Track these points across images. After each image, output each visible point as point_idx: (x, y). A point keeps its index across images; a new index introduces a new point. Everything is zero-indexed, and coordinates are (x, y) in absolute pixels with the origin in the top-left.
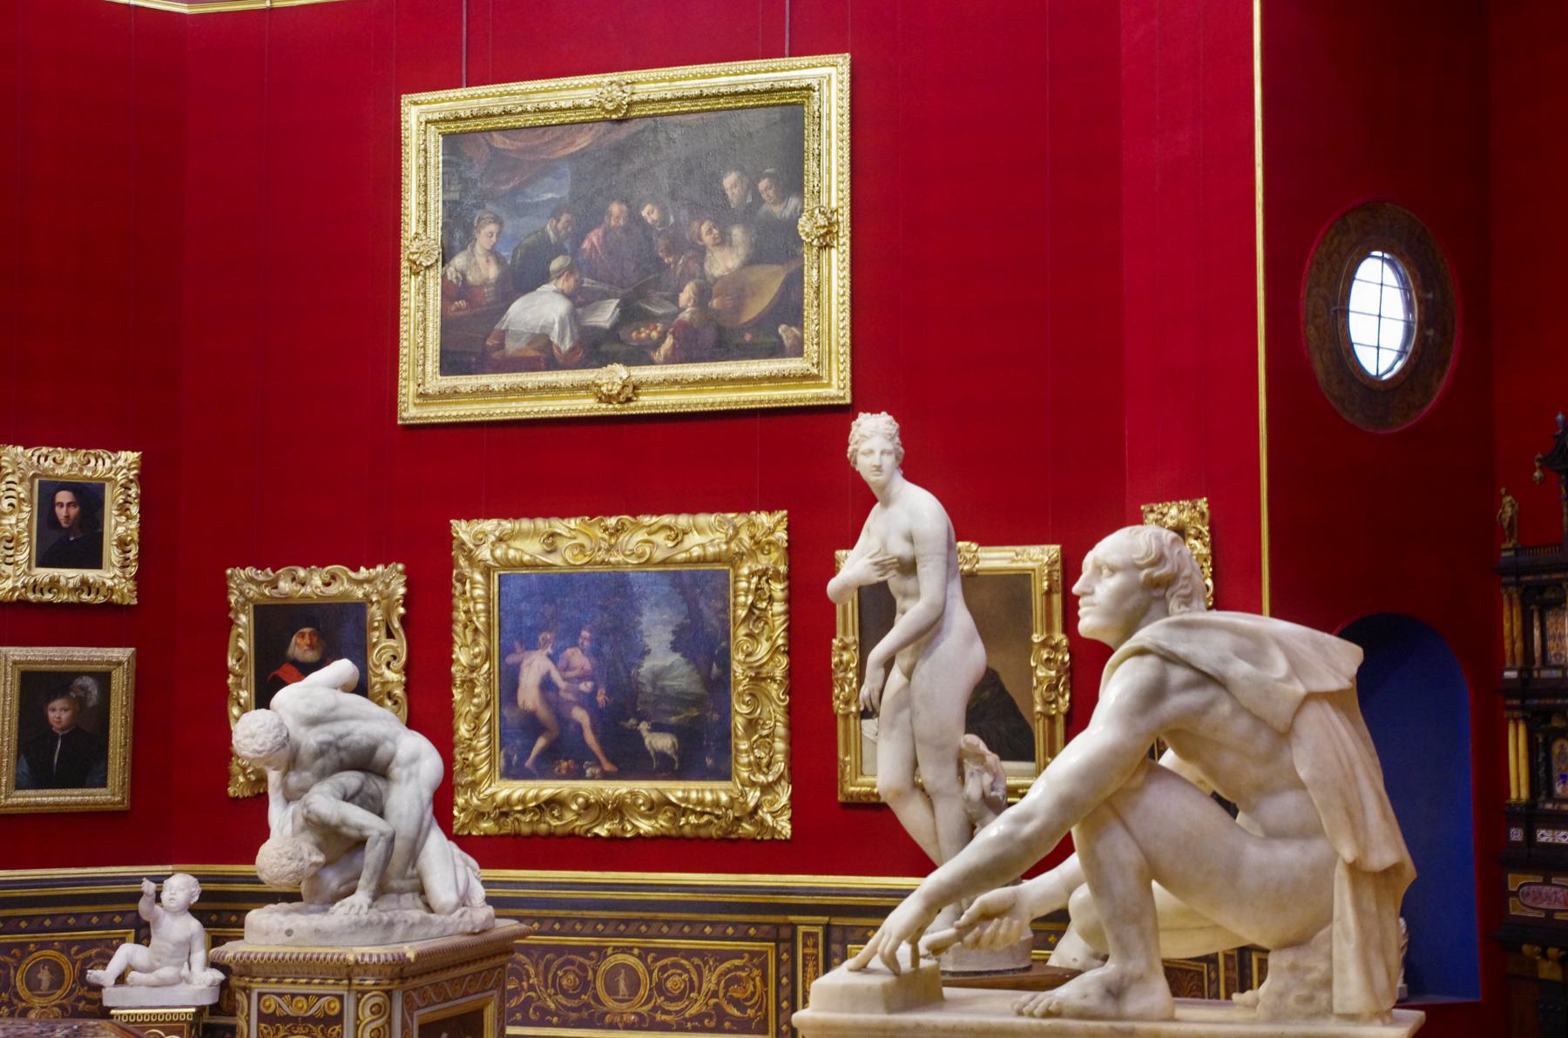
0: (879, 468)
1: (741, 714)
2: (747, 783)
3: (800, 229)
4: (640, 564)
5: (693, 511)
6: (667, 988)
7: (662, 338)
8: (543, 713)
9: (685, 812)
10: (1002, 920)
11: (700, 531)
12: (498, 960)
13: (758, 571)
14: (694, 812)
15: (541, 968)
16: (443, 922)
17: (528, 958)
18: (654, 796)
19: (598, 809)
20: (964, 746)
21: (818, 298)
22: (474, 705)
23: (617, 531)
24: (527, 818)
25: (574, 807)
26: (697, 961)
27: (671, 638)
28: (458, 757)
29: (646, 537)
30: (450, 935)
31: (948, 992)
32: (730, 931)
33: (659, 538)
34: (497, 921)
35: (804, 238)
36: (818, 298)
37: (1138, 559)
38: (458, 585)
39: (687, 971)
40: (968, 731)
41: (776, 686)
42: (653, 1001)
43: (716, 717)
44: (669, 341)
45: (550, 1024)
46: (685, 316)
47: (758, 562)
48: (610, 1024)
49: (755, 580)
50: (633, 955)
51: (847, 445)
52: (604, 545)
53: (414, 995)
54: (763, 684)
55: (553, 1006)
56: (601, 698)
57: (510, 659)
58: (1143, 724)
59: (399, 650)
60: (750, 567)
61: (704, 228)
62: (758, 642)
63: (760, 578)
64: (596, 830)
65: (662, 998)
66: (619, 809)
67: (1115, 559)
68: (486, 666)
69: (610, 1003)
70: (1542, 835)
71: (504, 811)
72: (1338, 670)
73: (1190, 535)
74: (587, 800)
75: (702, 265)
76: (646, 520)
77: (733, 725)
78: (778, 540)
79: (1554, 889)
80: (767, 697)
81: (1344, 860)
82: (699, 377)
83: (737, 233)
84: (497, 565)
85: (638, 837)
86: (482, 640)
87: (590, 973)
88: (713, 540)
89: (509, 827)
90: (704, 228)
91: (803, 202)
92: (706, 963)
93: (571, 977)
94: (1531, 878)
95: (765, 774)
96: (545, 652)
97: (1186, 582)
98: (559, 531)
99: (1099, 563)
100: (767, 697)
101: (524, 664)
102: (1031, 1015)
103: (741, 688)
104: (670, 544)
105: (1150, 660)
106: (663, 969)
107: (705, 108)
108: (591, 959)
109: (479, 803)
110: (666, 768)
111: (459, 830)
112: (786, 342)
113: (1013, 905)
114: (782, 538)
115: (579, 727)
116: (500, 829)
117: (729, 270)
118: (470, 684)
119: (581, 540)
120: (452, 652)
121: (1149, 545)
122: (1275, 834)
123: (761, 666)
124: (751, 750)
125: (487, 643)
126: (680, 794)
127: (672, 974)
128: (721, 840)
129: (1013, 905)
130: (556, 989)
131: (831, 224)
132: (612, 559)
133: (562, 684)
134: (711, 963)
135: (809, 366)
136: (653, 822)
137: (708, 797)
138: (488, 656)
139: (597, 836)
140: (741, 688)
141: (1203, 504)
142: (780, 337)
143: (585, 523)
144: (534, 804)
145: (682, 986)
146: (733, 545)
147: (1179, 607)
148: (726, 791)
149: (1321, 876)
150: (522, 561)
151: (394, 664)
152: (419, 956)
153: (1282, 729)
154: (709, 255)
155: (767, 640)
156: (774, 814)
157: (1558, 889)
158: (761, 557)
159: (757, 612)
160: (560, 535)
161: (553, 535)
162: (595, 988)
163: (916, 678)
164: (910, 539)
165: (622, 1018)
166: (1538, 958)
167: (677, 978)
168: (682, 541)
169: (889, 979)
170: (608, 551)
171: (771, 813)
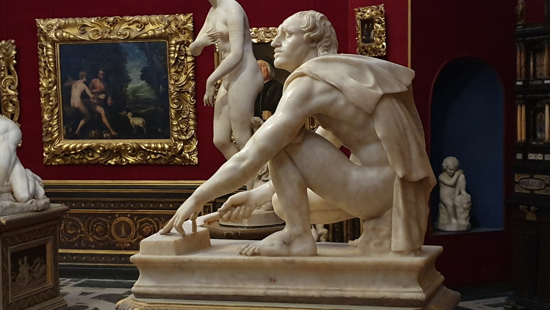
1: (173, 108)
2: (177, 140)
4: (124, 39)
5: (149, 14)
6: (143, 232)
8: (83, 109)
9: (149, 153)
10: (241, 207)
12: (52, 223)
15: (86, 223)
16: (21, 206)
17: (80, 219)
18: (135, 146)
19: (109, 152)
20: (253, 122)
22: (50, 106)
23: (114, 24)
24: (77, 157)
25: (99, 151)
26: (156, 219)
27: (141, 73)
28: (44, 129)
29: (127, 26)
30: (26, 212)
31: (213, 241)
32: (171, 206)
33: (133, 27)
34: (51, 205)
38: (40, 49)
39: (152, 224)
40: (255, 116)
41: (189, 95)
42: (137, 237)
43: (162, 110)
45: (91, 248)
48: (118, 247)
49: (178, 46)
50: (128, 217)
52: (108, 30)
53: (8, 240)
54: (183, 95)
55: (92, 240)
56: (109, 102)
57: (67, 84)
59: (14, 80)
60: (175, 40)
62: (181, 75)
64: (109, 162)
65: (141, 236)
66: (119, 152)
67: (291, 28)
68: (55, 87)
69: (118, 239)
70: (531, 156)
71: (67, 153)
72: (400, 82)
73: (376, 22)
74: (104, 148)
76: (127, 18)
77: (170, 113)
79: (534, 180)
80: (185, 100)
81: (398, 176)
84: (58, 40)
85: (128, 164)
86: (52, 75)
87: (108, 225)
88: (158, 28)
89: (69, 160)
92: (161, 220)
93: (100, 227)
94: (525, 176)
95: (185, 135)
96: (82, 81)
97: (327, 40)
98: (87, 24)
99: (284, 30)
100: (185, 100)
101: (73, 86)
102: (246, 254)
103: (173, 97)
104: (139, 30)
105: (306, 79)
106: (141, 223)
108: (109, 219)
109: (54, 150)
110: (138, 133)
111: (46, 163)
113: (248, 199)
114: (190, 26)
115: (100, 115)
116: (65, 162)
118: (47, 96)
119: (97, 28)
120: (40, 81)
121: (309, 21)
122: (366, 164)
123: (182, 86)
124: (178, 125)
125: (55, 76)
126: (146, 145)
127: (146, 225)
129: (248, 199)
130: (93, 233)
132: (112, 37)
133: (91, 96)
134: (163, 220)
136: (135, 158)
138: (55, 83)
139: (110, 164)
140: (173, 97)
141: (382, 7)
143: (99, 20)
144: (80, 150)
145: (150, 231)
147: (323, 52)
148: (167, 144)
149: (387, 184)
150: (69, 38)
151: (12, 87)
152: (8, 222)
153: (370, 112)
157: (536, 180)
158: (181, 35)
159: (180, 61)
160: (87, 26)
161: (84, 26)
162: (110, 232)
163: (230, 90)
164: (226, 23)
165: (123, 245)
166: (526, 211)
167: (148, 227)
168: (144, 28)
169: (178, 238)
170: (109, 33)
171: (188, 153)
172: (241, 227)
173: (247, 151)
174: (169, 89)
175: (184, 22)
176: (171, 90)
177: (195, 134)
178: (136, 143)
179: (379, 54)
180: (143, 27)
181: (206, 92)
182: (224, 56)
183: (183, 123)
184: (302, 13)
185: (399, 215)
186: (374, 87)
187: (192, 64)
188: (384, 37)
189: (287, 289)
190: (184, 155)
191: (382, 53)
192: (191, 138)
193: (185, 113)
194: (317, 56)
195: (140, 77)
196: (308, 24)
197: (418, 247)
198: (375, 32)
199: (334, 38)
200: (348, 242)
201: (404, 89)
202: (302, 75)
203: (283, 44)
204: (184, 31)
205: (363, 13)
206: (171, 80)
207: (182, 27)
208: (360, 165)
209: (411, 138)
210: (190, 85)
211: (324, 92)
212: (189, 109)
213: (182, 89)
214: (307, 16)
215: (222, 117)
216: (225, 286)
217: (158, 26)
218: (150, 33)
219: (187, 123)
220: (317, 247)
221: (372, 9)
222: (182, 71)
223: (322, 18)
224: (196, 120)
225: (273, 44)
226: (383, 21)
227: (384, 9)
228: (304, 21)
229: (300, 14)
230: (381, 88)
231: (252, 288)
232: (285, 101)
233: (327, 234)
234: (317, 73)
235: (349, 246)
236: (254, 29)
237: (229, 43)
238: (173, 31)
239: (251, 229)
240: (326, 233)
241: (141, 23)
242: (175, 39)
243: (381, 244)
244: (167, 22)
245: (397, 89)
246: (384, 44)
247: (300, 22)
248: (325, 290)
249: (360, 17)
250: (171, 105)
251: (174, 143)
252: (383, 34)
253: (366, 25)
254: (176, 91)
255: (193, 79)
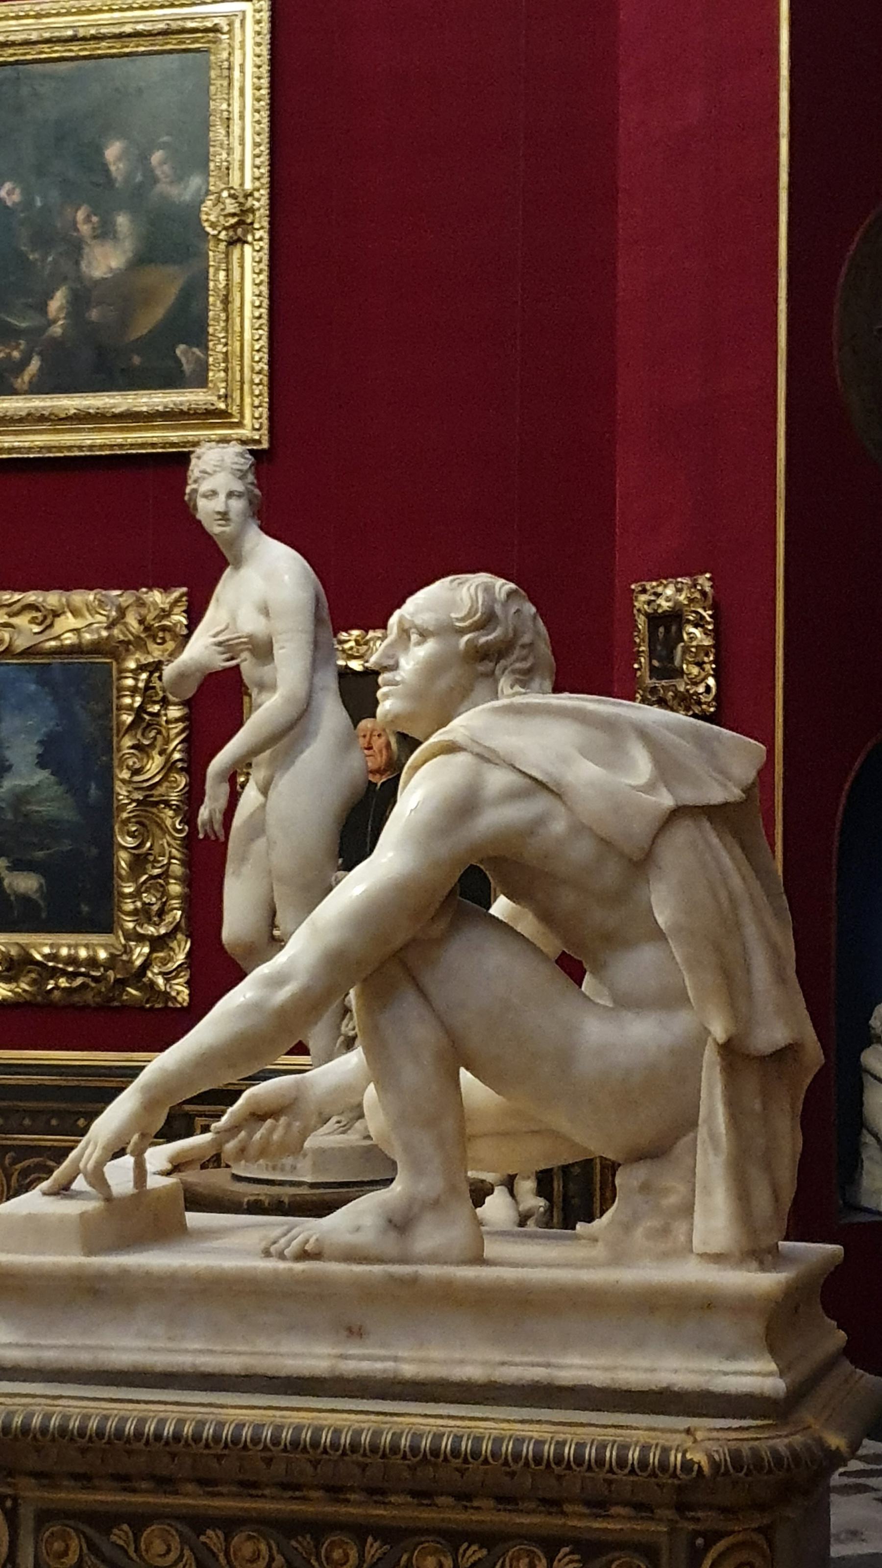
0: (224, 516)
1: (125, 848)
3: (204, 217)
5: (67, 586)
7: (25, 362)
9: (54, 973)
10: (277, 1120)
11: (76, 613)
13: (149, 664)
14: (64, 973)
18: (13, 952)
21: (225, 310)
31: (193, 1219)
33: (22, 621)
35: (209, 229)
36: (225, 310)
37: (458, 620)
41: (171, 813)
44: (35, 364)
46: (57, 330)
47: (148, 653)
49: (144, 676)
51: (185, 483)
54: (155, 810)
58: (443, 849)
60: (137, 660)
61: (81, 215)
63: (151, 674)
67: (425, 619)
72: (723, 772)
73: (688, 621)
75: (77, 263)
77: (115, 861)
78: (175, 625)
80: (159, 825)
81: (715, 1040)
82: (73, 411)
83: (122, 221)
90: (81, 215)
91: (208, 183)
97: (525, 652)
99: (407, 626)
100: (159, 825)
102: (282, 1256)
103: (125, 815)
104: (37, 629)
105: (461, 759)
107: (82, 53)
112: (186, 367)
114: (180, 622)
117: (111, 270)
121: (474, 601)
123: (153, 787)
126: (47, 950)
128: (99, 1008)
129: (296, 1099)
131: (244, 212)
135: (215, 398)
136: (13, 986)
137: (83, 953)
141: (704, 581)
142: (178, 361)
146: (116, 631)
147: (512, 687)
148: (105, 947)
153: (637, 856)
154: (86, 250)
155: (160, 754)
156: (168, 977)
158: (152, 646)
163: (272, 794)
164: (265, 611)
168: (51, 626)
172: (293, 1184)
173: (291, 960)
174: (115, 796)
175: (163, 610)
176: (121, 797)
177: (183, 921)
178: (17, 944)
179: (697, 709)
180: (48, 622)
181: (206, 799)
182: (259, 701)
183: (152, 891)
184: (454, 580)
185: (716, 1149)
186: (650, 788)
187: (181, 725)
188: (711, 663)
189: (396, 1359)
190: (150, 979)
191: (704, 706)
192: (171, 932)
193: (159, 862)
194: (497, 698)
195: (37, 761)
196: (470, 609)
197: (766, 1241)
198: (686, 650)
199: (545, 649)
200: (574, 1228)
201: (735, 794)
202: (451, 748)
203: (403, 662)
204: (161, 634)
205: (653, 598)
206: (121, 771)
207: (157, 625)
208: (611, 1006)
209: (751, 930)
210: (175, 785)
211: (512, 795)
212: (170, 852)
213: (152, 796)
214: (469, 589)
215: (247, 869)
216: (218, 1348)
217: (90, 620)
218: (66, 639)
219: (161, 889)
220: (484, 1237)
221: (679, 586)
222: (152, 746)
223: (510, 594)
224: (187, 881)
225: (376, 663)
226: (708, 619)
227: (712, 587)
228: (461, 599)
229: (452, 581)
230: (669, 790)
231: (295, 1356)
232: (404, 820)
233: (546, 1211)
234: (492, 744)
235: (577, 1237)
236: (355, 633)
237: (272, 665)
238: (132, 634)
239: (322, 1191)
240: (542, 1209)
241: (45, 613)
242: (137, 656)
243: (665, 1231)
244: (114, 609)
245: (716, 795)
246: (711, 681)
247: (453, 604)
248: (503, 1364)
249: (646, 606)
250: (119, 839)
251: (125, 946)
252: (707, 655)
253: (661, 629)
254: (133, 801)
255: (182, 769)
